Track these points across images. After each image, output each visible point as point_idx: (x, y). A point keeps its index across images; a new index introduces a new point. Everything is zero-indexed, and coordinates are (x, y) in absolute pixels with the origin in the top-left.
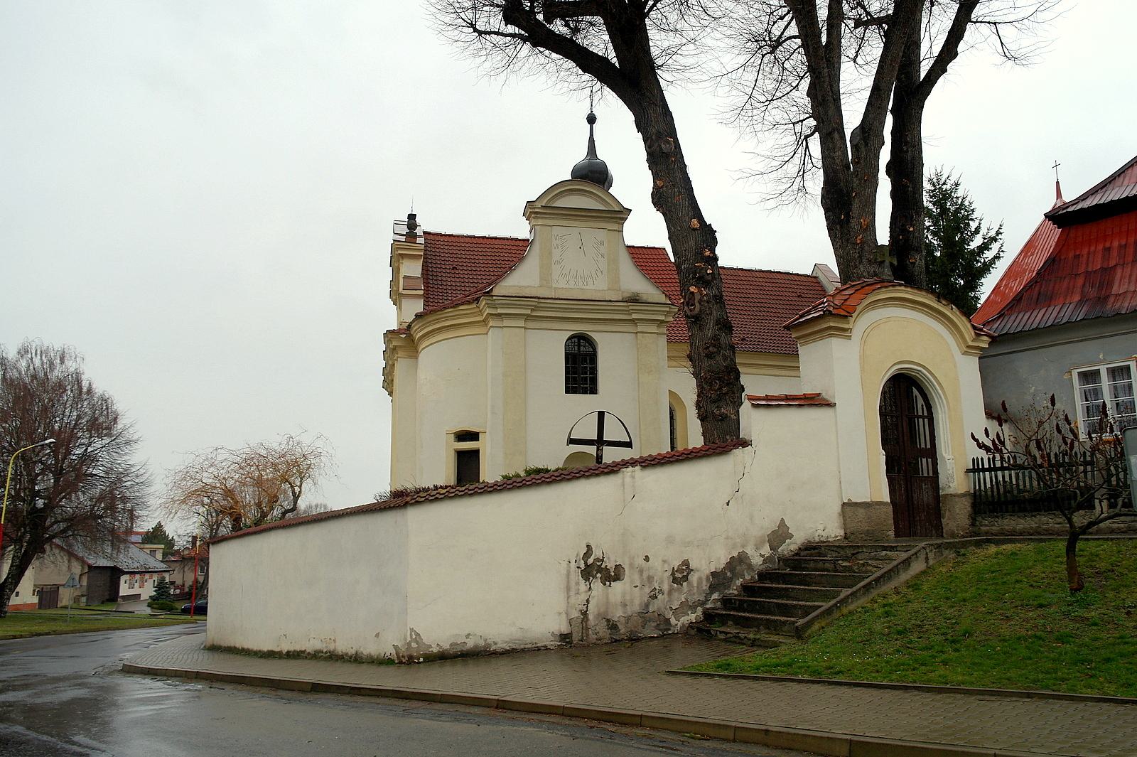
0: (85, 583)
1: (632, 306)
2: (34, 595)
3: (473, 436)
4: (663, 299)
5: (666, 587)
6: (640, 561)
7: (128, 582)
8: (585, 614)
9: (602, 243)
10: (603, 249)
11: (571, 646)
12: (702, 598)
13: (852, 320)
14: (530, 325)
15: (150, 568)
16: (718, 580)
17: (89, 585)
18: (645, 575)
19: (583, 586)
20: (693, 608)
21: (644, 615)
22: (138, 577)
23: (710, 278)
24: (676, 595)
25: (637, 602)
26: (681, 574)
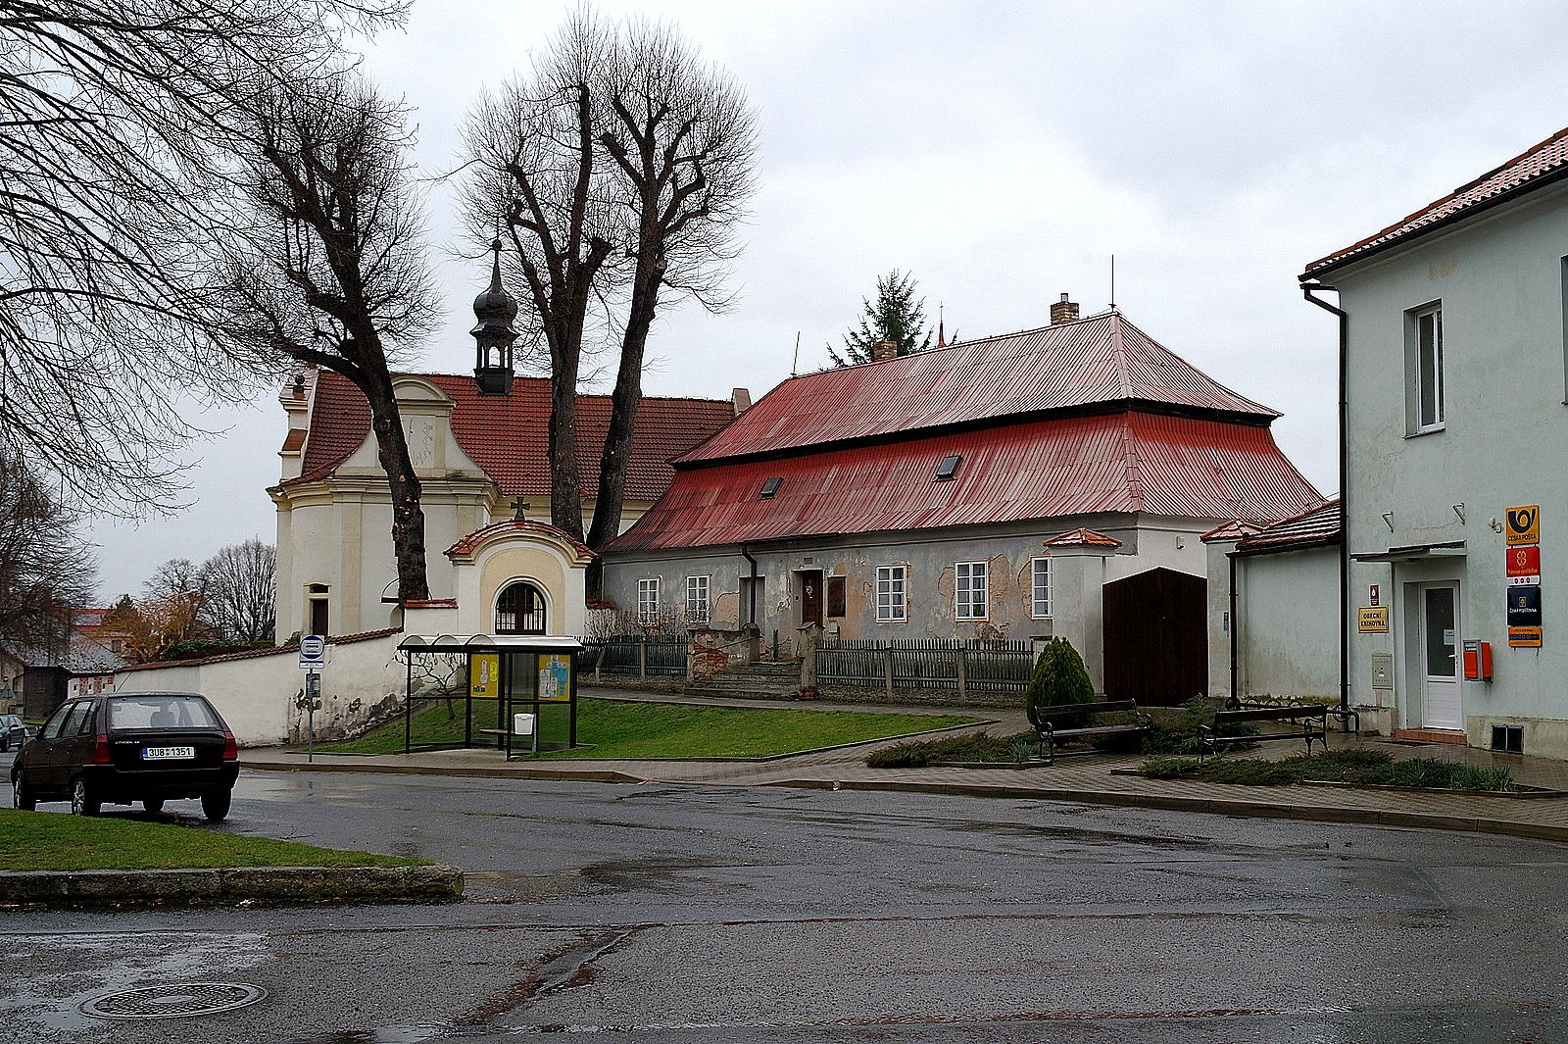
0: (20, 689)
1: (452, 484)
2: (1521, 523)
3: (324, 589)
4: (482, 475)
5: (345, 714)
6: (332, 699)
7: (78, 688)
8: (298, 728)
9: (431, 428)
10: (432, 433)
11: (287, 744)
12: (365, 720)
13: (473, 555)
14: (365, 500)
15: (108, 669)
16: (376, 710)
17: (25, 692)
18: (334, 707)
19: (297, 712)
20: (359, 726)
21: (331, 729)
22: (91, 681)
23: (406, 517)
24: (350, 718)
25: (327, 721)
26: (355, 706)
